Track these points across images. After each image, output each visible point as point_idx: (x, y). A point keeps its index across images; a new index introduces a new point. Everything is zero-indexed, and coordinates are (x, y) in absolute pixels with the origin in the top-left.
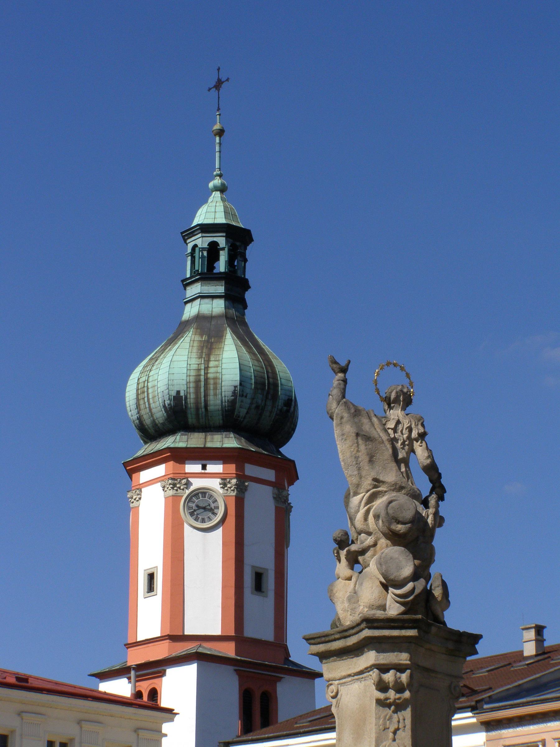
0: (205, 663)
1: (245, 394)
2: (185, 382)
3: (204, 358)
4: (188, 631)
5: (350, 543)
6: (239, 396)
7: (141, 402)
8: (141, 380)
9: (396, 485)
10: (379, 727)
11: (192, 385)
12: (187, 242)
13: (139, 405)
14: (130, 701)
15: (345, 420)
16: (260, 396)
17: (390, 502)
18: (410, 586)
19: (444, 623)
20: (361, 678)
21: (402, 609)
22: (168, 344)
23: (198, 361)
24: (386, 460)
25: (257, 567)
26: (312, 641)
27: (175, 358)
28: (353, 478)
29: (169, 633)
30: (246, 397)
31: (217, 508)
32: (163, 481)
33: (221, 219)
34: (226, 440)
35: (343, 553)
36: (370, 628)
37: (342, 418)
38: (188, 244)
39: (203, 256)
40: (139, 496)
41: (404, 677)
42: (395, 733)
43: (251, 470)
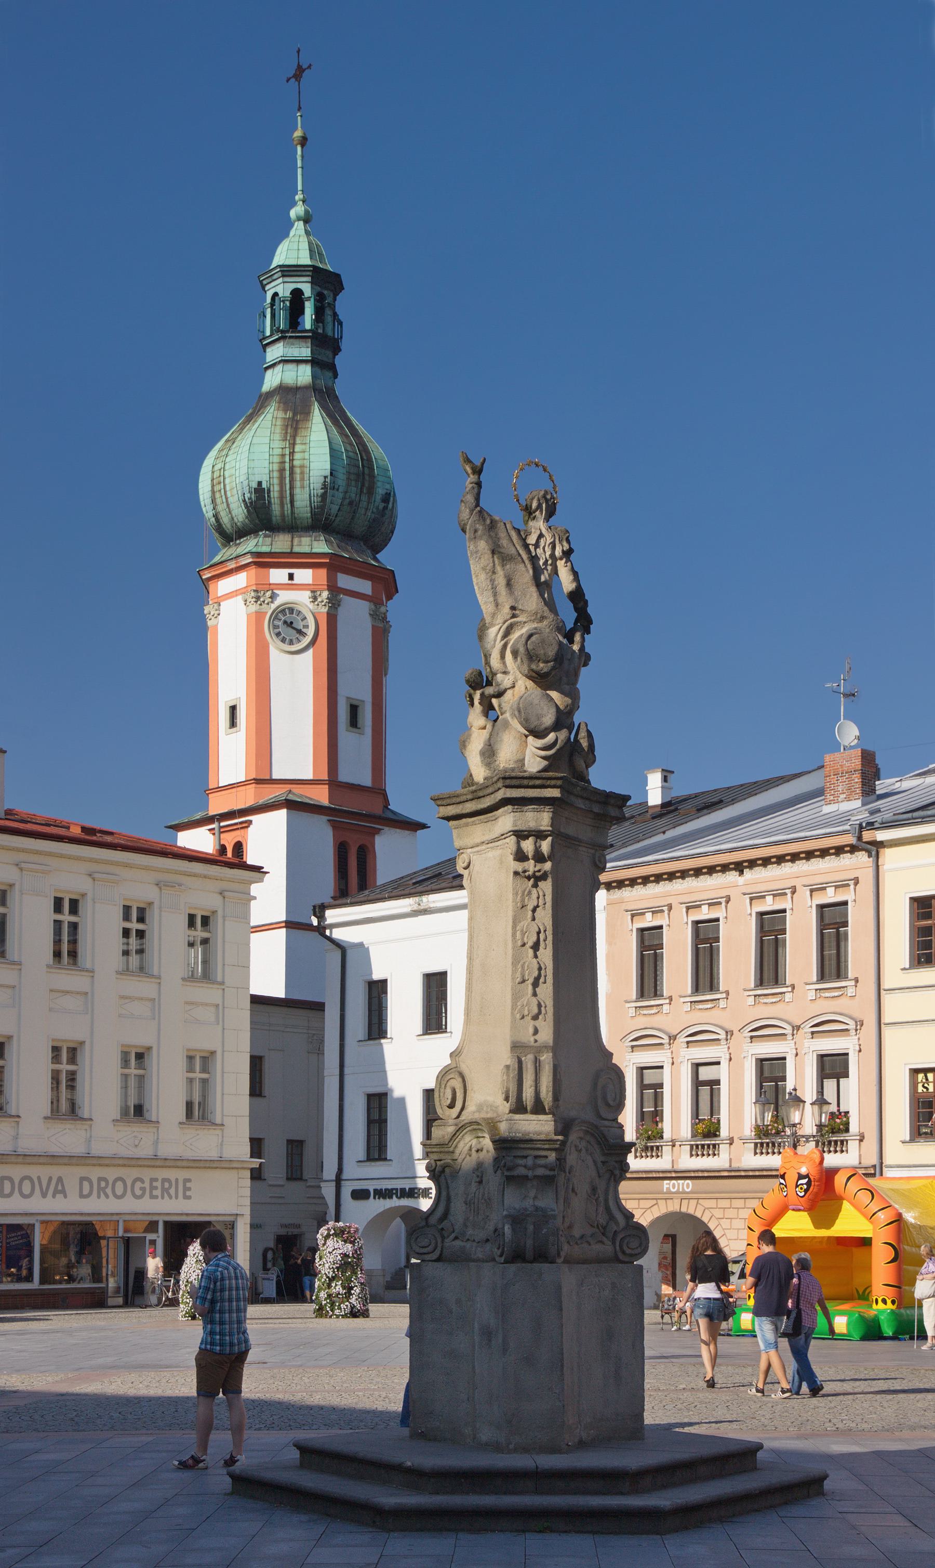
1: (336, 487)
2: (267, 472)
3: (289, 440)
4: (275, 776)
5: (484, 685)
7: (217, 495)
8: (217, 468)
9: (537, 615)
10: (517, 904)
11: (276, 474)
12: (266, 289)
13: (215, 499)
14: (212, 857)
15: (479, 533)
16: (354, 489)
17: (530, 636)
18: (552, 736)
19: (588, 782)
21: (545, 763)
22: (246, 422)
23: (282, 444)
25: (353, 699)
26: (439, 802)
27: (255, 440)
29: (254, 777)
30: (338, 490)
31: (307, 627)
33: (305, 260)
34: (315, 544)
36: (507, 787)
37: (476, 531)
38: (267, 292)
40: (217, 612)
41: (545, 846)
42: (534, 910)
43: (344, 581)
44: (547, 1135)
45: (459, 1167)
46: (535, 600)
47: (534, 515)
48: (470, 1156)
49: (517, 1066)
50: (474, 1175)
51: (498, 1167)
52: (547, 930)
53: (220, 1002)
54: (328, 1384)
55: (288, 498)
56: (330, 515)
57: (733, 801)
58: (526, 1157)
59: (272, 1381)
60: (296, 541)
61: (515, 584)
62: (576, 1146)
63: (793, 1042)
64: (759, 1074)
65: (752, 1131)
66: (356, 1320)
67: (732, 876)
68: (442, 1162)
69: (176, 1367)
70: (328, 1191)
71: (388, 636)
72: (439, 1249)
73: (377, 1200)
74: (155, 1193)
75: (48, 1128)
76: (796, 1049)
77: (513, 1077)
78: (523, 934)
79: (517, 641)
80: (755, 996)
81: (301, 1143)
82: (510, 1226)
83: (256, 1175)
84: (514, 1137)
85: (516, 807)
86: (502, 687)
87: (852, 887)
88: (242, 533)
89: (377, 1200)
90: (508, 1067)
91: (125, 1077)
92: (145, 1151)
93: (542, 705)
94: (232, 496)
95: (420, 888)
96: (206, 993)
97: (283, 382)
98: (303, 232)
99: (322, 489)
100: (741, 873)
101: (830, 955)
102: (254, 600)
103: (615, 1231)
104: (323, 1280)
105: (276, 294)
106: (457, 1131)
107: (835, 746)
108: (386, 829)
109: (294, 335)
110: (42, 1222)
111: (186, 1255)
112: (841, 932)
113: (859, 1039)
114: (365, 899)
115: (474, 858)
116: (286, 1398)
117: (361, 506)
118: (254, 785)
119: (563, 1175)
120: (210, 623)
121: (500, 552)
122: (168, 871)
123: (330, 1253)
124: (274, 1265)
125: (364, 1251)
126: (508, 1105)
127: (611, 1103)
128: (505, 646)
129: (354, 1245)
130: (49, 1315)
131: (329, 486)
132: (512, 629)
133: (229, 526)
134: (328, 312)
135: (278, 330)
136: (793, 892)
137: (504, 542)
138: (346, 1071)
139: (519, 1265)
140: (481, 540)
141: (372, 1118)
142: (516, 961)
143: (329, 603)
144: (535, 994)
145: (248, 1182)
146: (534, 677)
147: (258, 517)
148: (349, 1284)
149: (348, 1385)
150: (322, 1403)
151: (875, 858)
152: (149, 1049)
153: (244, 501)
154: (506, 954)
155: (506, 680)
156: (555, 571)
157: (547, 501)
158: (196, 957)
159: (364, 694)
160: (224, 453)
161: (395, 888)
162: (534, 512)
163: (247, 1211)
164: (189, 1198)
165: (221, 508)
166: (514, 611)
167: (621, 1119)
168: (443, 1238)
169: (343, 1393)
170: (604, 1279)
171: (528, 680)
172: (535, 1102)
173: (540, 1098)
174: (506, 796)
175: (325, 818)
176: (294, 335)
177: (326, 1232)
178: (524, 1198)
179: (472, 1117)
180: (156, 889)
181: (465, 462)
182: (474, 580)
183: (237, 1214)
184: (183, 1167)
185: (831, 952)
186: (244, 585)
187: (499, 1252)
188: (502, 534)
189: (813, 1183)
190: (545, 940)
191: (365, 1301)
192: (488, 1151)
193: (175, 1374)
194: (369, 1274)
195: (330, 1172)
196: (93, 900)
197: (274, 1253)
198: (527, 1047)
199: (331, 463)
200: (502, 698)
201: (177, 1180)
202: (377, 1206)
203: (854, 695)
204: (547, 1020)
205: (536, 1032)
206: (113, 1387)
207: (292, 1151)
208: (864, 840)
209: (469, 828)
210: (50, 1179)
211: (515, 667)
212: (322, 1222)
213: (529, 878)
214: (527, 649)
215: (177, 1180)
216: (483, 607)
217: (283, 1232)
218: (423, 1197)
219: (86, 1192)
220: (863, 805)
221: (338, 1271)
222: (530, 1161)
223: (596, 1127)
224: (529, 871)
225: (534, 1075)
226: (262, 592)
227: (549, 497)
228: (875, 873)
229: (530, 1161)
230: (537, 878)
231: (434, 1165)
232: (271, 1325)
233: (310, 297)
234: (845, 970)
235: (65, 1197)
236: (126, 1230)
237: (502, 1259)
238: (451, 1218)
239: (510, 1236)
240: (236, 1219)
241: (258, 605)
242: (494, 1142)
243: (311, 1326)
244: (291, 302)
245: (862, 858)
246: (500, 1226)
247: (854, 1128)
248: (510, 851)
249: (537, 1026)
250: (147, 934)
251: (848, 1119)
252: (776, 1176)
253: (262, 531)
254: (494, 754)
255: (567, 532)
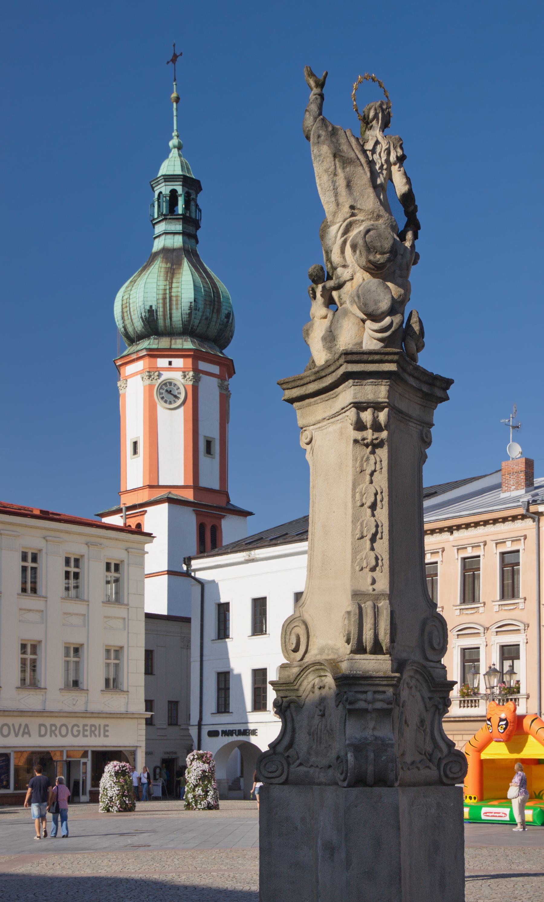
0: (172, 505)
1: (198, 309)
2: (155, 299)
4: (161, 483)
5: (325, 280)
6: (194, 310)
7: (125, 314)
8: (125, 298)
9: (373, 213)
11: (161, 301)
15: (322, 138)
16: (209, 310)
17: (368, 231)
18: (387, 320)
20: (337, 421)
23: (165, 283)
24: (364, 185)
26: (285, 386)
27: (148, 281)
28: (330, 206)
30: (199, 310)
31: (180, 393)
32: (142, 373)
34: (185, 343)
35: (319, 289)
36: (348, 362)
37: (319, 136)
39: (166, 200)
40: (125, 385)
41: (382, 416)
42: (372, 474)
43: (203, 366)
44: (385, 673)
45: (303, 703)
46: (372, 200)
47: (371, 124)
48: (313, 693)
49: (357, 611)
50: (317, 709)
51: (340, 702)
52: (384, 491)
53: (126, 617)
54: (192, 865)
55: (168, 316)
56: (194, 326)
57: (444, 492)
58: (366, 692)
59: (151, 863)
60: (173, 341)
61: (354, 185)
62: (407, 683)
63: (484, 637)
64: (462, 658)
65: (458, 693)
66: (211, 811)
67: (446, 535)
68: (288, 698)
69: (88, 850)
70: (193, 732)
71: (229, 400)
72: (285, 773)
73: (223, 737)
74: (86, 733)
75: (19, 694)
76: (486, 642)
77: (354, 621)
78: (362, 495)
79: (356, 236)
80: (460, 609)
81: (177, 703)
82: (352, 754)
83: (149, 722)
84: (356, 674)
85: (356, 381)
86: (342, 280)
87: (522, 541)
88: (141, 337)
89: (223, 737)
90: (349, 613)
91: (67, 662)
92: (80, 707)
93: (379, 291)
94: (134, 314)
95: (250, 546)
96: (118, 611)
97: (165, 246)
98: (177, 155)
99: (189, 310)
100: (452, 533)
101: (508, 584)
102: (148, 377)
103: (440, 758)
104: (190, 787)
105: (161, 193)
106: (302, 671)
107: (507, 458)
108: (228, 515)
109: (171, 217)
110: (15, 752)
111: (103, 772)
112: (515, 569)
113: (526, 635)
114: (216, 553)
115: (316, 435)
116: (161, 878)
117: (213, 320)
118: (148, 489)
119: (398, 708)
120: (121, 392)
121: (341, 156)
122: (93, 536)
123: (195, 770)
124: (160, 777)
125: (216, 768)
126: (349, 648)
127: (436, 647)
128: (344, 243)
129: (209, 765)
130: (18, 810)
131: (193, 308)
132: (351, 227)
133: (132, 333)
134: (192, 203)
135: (162, 214)
136: (485, 545)
137: (345, 147)
138: (205, 658)
139: (361, 788)
140: (324, 144)
141: (220, 687)
142: (355, 520)
143: (193, 379)
144: (372, 549)
145: (144, 726)
146: (371, 269)
147: (150, 327)
148: (206, 789)
149: (206, 866)
150: (187, 883)
151: (537, 523)
152: (82, 645)
153: (142, 317)
154: (346, 514)
155: (346, 273)
156: (390, 177)
157: (383, 111)
158: (111, 589)
159: (215, 434)
160: (129, 289)
161: (235, 547)
162: (371, 122)
163: (143, 744)
164: (107, 736)
165: (128, 322)
166: (353, 211)
167: (444, 661)
168: (289, 764)
169: (202, 874)
170: (430, 800)
171: (365, 272)
172: (374, 643)
173: (378, 640)
174: (347, 370)
175: (191, 509)
176: (171, 217)
177: (192, 757)
178: (365, 729)
179: (314, 659)
180: (86, 547)
181: (309, 75)
182: (318, 181)
183: (137, 746)
184: (103, 718)
185: (508, 581)
186: (142, 368)
187: (342, 777)
188: (343, 141)
189: (509, 724)
190: (381, 501)
191: (216, 799)
192: (330, 688)
193: (85, 856)
194: (219, 782)
195: (194, 720)
196: (47, 553)
197: (161, 770)
198: (366, 594)
199: (195, 294)
200: (342, 290)
201: (100, 725)
202: (223, 741)
203: (518, 427)
204: (384, 571)
205: (374, 582)
206: (38, 868)
207: (171, 707)
208: (531, 511)
209: (311, 408)
210: (20, 725)
211: (353, 260)
212: (190, 750)
213: (367, 446)
214: (365, 242)
215: (100, 725)
216: (325, 207)
217: (166, 756)
218: (252, 735)
219: (43, 732)
220: (526, 492)
221: (199, 781)
222: (370, 696)
223: (425, 667)
224: (367, 439)
225: (373, 619)
226: (153, 373)
227: (384, 107)
228: (537, 532)
229: (370, 696)
230: (375, 446)
231: (280, 701)
232: (157, 816)
233: (181, 194)
234: (517, 593)
235: (30, 736)
236: (68, 756)
237: (345, 784)
238: (295, 746)
239: (353, 763)
240: (137, 749)
241: (150, 381)
242: (336, 679)
243: (182, 816)
244: (170, 197)
245: (529, 522)
246: (342, 754)
247: (523, 690)
248: (350, 421)
249: (375, 576)
250: (81, 576)
251: (519, 685)
252: (485, 721)
253: (152, 335)
254: (334, 339)
255: (401, 139)
